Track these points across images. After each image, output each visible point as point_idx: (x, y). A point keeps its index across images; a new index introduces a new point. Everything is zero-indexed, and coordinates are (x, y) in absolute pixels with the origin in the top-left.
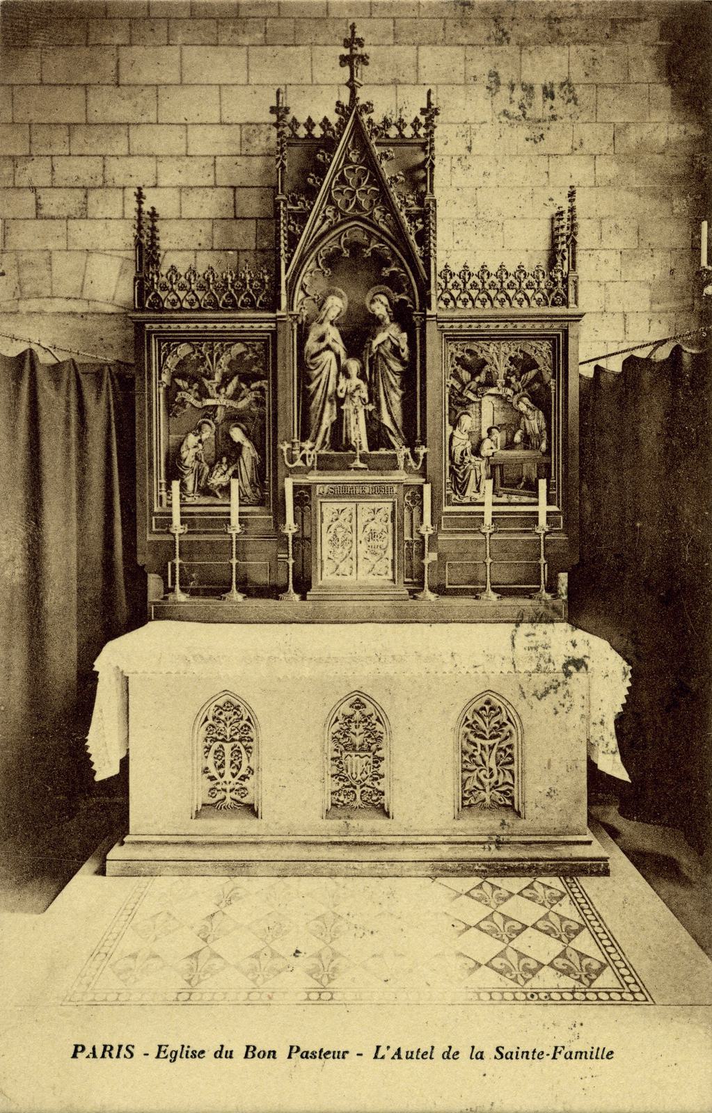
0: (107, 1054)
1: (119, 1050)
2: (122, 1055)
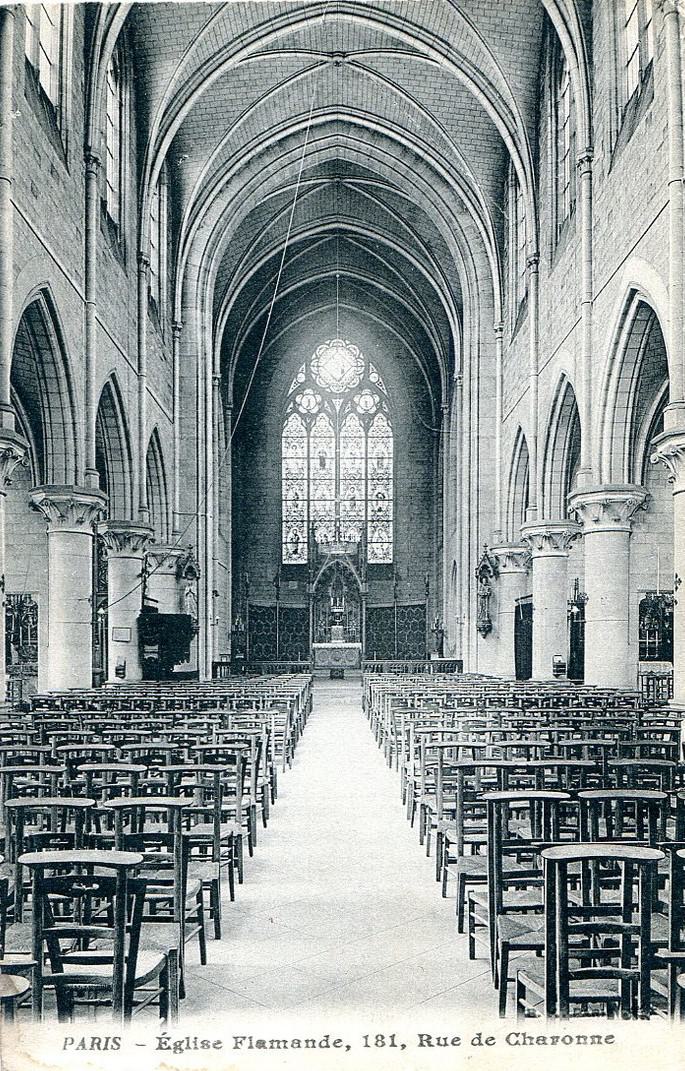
0: (95, 1046)
1: (107, 1042)
2: (109, 1047)
